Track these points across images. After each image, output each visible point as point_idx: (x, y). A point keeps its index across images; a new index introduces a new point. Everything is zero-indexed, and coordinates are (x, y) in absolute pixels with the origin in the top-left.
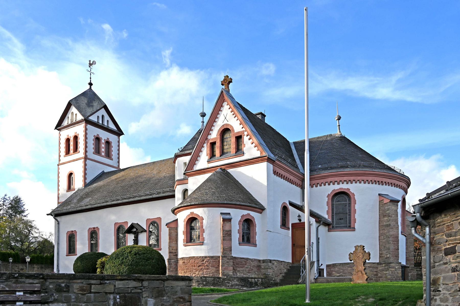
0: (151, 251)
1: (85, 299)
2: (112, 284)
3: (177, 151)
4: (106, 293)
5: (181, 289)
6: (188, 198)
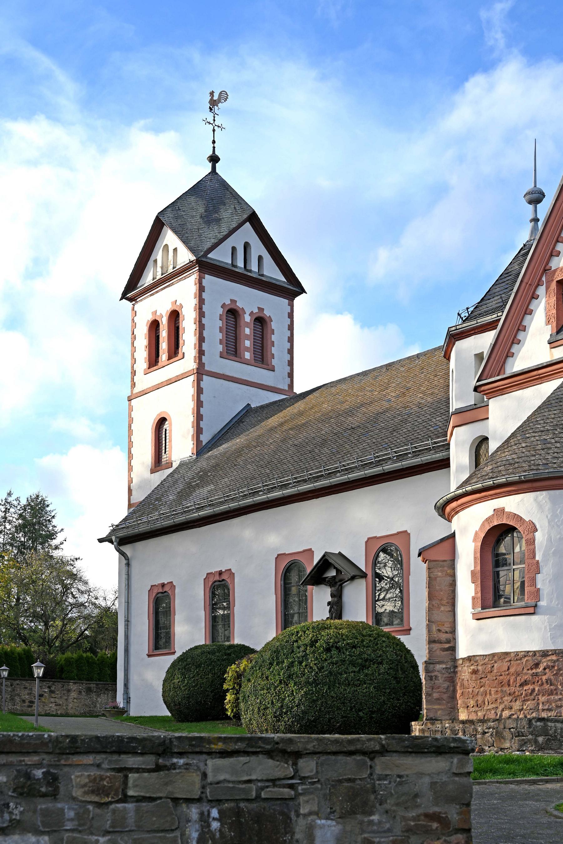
0: (375, 639)
1: (108, 822)
2: (196, 768)
3: (453, 321)
4: (176, 800)
5: (433, 784)
6: (486, 465)
